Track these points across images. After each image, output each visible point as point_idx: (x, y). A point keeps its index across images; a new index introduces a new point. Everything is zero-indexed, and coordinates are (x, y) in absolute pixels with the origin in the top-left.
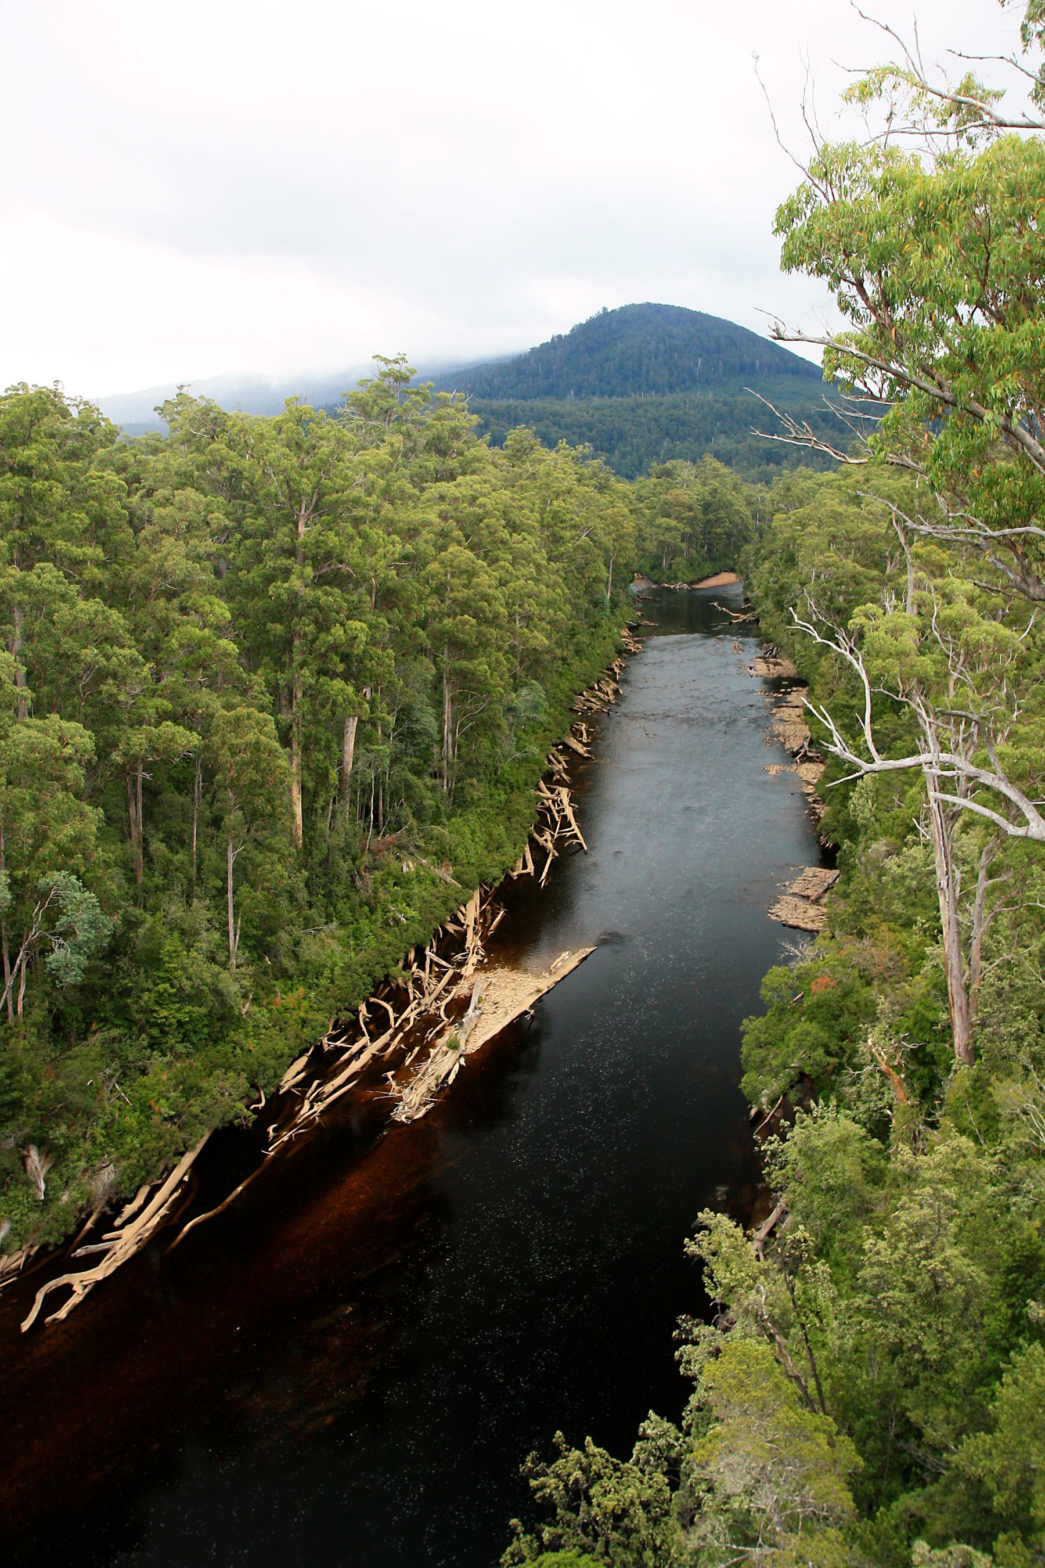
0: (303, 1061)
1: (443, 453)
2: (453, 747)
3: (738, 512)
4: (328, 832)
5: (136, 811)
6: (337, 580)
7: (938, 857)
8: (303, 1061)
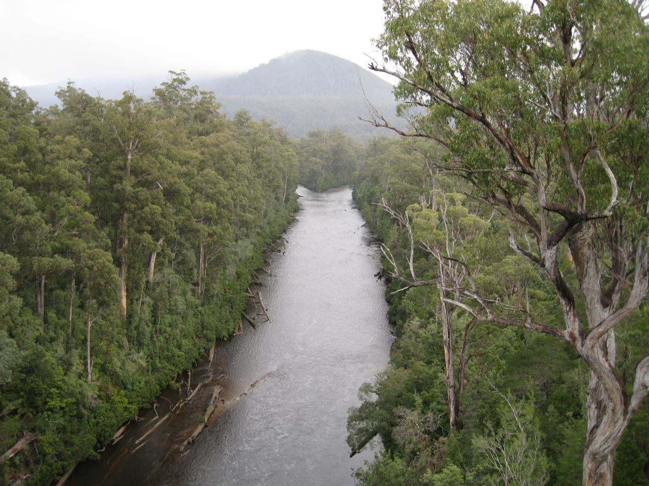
0: (122, 429)
1: (203, 121)
2: (204, 270)
3: (350, 156)
4: (139, 312)
5: (41, 300)
6: (149, 184)
7: (445, 329)
8: (122, 429)
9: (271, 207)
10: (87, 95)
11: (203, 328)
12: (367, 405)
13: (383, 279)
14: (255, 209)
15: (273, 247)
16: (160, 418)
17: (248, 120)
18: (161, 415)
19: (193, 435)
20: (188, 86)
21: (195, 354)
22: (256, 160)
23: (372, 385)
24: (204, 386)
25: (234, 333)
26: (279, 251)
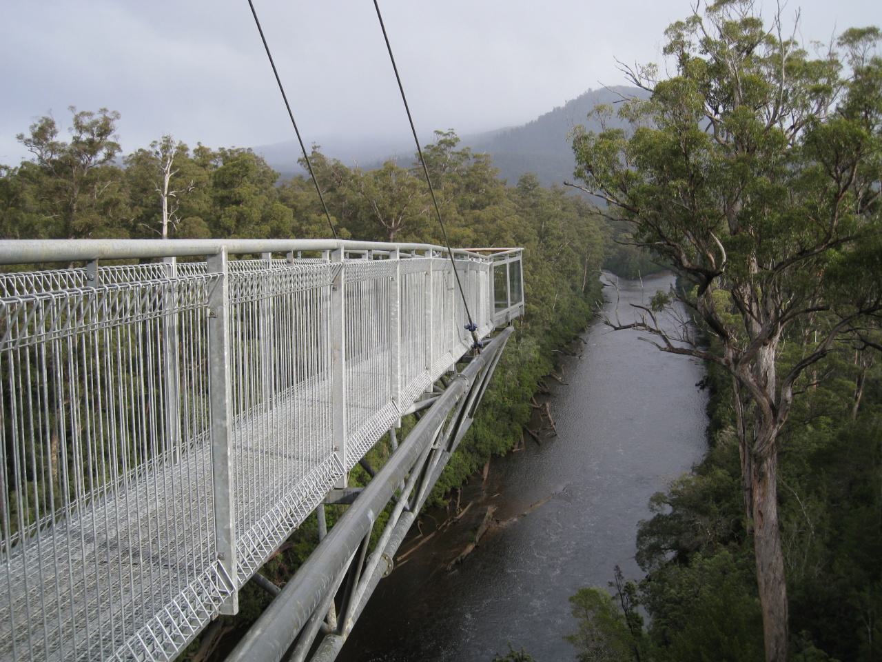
1: (476, 191)
9: (566, 298)
10: (342, 167)
11: (476, 441)
12: (659, 519)
13: (707, 390)
14: (543, 299)
15: (567, 349)
16: (425, 536)
17: (535, 186)
18: (425, 535)
19: (462, 554)
20: (458, 148)
21: (465, 470)
22: (544, 238)
23: (666, 495)
24: (475, 506)
25: (513, 448)
26: (575, 354)
